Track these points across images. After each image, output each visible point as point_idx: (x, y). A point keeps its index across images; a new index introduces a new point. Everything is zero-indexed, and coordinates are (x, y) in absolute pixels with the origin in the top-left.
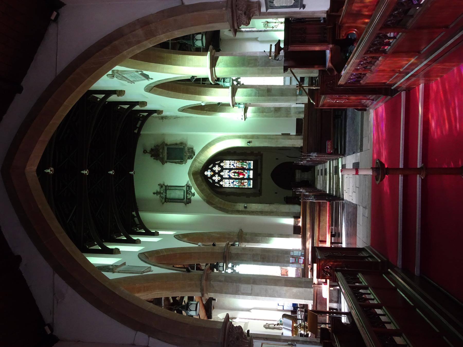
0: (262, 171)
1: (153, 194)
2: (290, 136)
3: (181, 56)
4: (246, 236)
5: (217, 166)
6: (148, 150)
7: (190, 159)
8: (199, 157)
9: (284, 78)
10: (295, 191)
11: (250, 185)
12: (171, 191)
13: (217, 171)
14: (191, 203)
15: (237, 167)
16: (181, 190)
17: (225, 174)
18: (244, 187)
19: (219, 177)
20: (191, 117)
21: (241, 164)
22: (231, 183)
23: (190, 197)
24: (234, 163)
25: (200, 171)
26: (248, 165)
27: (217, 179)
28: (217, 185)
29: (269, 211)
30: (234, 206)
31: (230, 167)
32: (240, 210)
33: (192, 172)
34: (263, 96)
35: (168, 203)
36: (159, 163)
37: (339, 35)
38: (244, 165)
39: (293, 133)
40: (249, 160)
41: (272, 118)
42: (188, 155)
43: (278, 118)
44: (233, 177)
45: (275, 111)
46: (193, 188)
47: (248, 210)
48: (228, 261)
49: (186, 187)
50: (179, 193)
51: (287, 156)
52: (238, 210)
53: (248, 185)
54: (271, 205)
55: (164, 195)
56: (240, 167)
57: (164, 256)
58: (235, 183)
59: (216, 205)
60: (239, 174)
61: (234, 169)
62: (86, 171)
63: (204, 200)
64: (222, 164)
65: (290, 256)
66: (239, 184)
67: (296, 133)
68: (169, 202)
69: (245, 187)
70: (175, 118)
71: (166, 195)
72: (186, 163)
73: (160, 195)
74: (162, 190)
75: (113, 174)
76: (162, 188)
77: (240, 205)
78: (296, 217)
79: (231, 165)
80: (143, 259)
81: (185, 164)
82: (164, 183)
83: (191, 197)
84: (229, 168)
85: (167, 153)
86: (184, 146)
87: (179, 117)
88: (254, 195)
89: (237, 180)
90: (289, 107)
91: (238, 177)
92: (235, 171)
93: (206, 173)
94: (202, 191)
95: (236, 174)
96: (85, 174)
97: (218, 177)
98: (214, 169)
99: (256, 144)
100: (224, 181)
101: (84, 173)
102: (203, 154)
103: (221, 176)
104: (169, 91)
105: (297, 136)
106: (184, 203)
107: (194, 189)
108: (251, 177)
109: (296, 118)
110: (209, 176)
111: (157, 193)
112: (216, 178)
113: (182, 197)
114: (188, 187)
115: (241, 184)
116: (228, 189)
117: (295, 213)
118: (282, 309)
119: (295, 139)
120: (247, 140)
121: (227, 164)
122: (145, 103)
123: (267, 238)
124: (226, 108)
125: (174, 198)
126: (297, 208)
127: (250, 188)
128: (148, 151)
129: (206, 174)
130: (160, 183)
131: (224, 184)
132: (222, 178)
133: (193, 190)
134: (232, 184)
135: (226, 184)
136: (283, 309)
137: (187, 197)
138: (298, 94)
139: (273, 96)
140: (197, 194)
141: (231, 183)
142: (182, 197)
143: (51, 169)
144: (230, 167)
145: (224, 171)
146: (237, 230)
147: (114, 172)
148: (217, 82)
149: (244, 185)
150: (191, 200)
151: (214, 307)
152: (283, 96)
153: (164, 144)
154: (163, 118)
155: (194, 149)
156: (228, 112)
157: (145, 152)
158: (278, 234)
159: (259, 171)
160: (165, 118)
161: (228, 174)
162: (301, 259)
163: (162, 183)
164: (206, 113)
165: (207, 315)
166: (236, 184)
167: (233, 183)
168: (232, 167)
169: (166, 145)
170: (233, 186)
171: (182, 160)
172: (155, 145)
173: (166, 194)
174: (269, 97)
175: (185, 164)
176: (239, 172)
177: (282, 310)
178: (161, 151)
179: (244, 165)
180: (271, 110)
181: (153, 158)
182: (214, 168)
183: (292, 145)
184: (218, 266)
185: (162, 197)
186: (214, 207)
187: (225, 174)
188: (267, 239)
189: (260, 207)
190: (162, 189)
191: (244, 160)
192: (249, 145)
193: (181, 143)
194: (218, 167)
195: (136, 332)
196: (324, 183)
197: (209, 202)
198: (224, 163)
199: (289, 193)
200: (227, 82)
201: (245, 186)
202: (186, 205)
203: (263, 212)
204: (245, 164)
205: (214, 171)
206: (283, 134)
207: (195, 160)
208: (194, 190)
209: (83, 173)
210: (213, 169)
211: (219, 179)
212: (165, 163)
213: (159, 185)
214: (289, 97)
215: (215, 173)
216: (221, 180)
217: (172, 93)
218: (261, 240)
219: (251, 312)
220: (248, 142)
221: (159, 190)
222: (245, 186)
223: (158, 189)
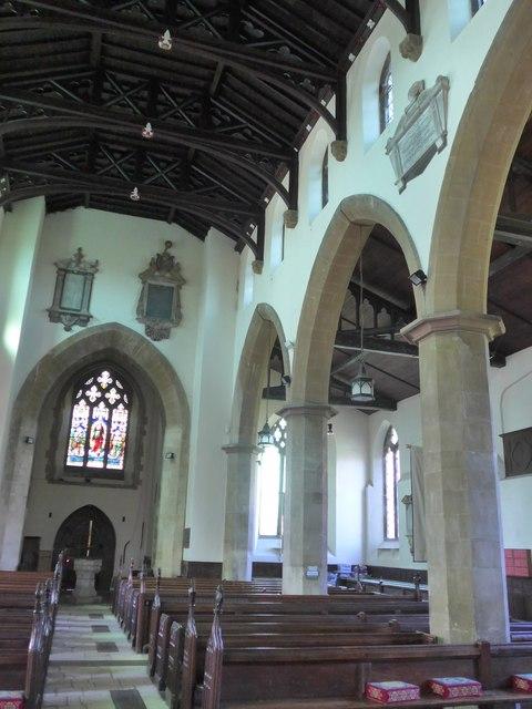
0: (96, 485)
5: (118, 397)
6: (172, 251)
11: (74, 460)
13: (107, 395)
17: (101, 412)
44: (93, 427)
47: (20, 444)
53: (74, 458)
58: (80, 429)
61: (109, 431)
64: (121, 406)
88: (51, 469)
91: (92, 436)
93: (106, 374)
95: (98, 433)
98: (113, 391)
103: (96, 404)
108: (90, 464)
110: (100, 380)
111: (80, 255)
112: (93, 394)
113: (65, 305)
116: (69, 413)
127: (66, 461)
132: (92, 405)
133: (77, 329)
135: (80, 412)
142: (65, 305)
153: (182, 282)
157: (169, 244)
161: (100, 418)
166: (77, 433)
168: (114, 426)
169: (180, 287)
170: (73, 425)
178: (168, 275)
183: (161, 553)
185: (69, 263)
191: (126, 450)
193: (180, 317)
197: (49, 361)
199: (47, 545)
204: (118, 453)
205: (107, 390)
217: (326, 270)
223: (89, 257)
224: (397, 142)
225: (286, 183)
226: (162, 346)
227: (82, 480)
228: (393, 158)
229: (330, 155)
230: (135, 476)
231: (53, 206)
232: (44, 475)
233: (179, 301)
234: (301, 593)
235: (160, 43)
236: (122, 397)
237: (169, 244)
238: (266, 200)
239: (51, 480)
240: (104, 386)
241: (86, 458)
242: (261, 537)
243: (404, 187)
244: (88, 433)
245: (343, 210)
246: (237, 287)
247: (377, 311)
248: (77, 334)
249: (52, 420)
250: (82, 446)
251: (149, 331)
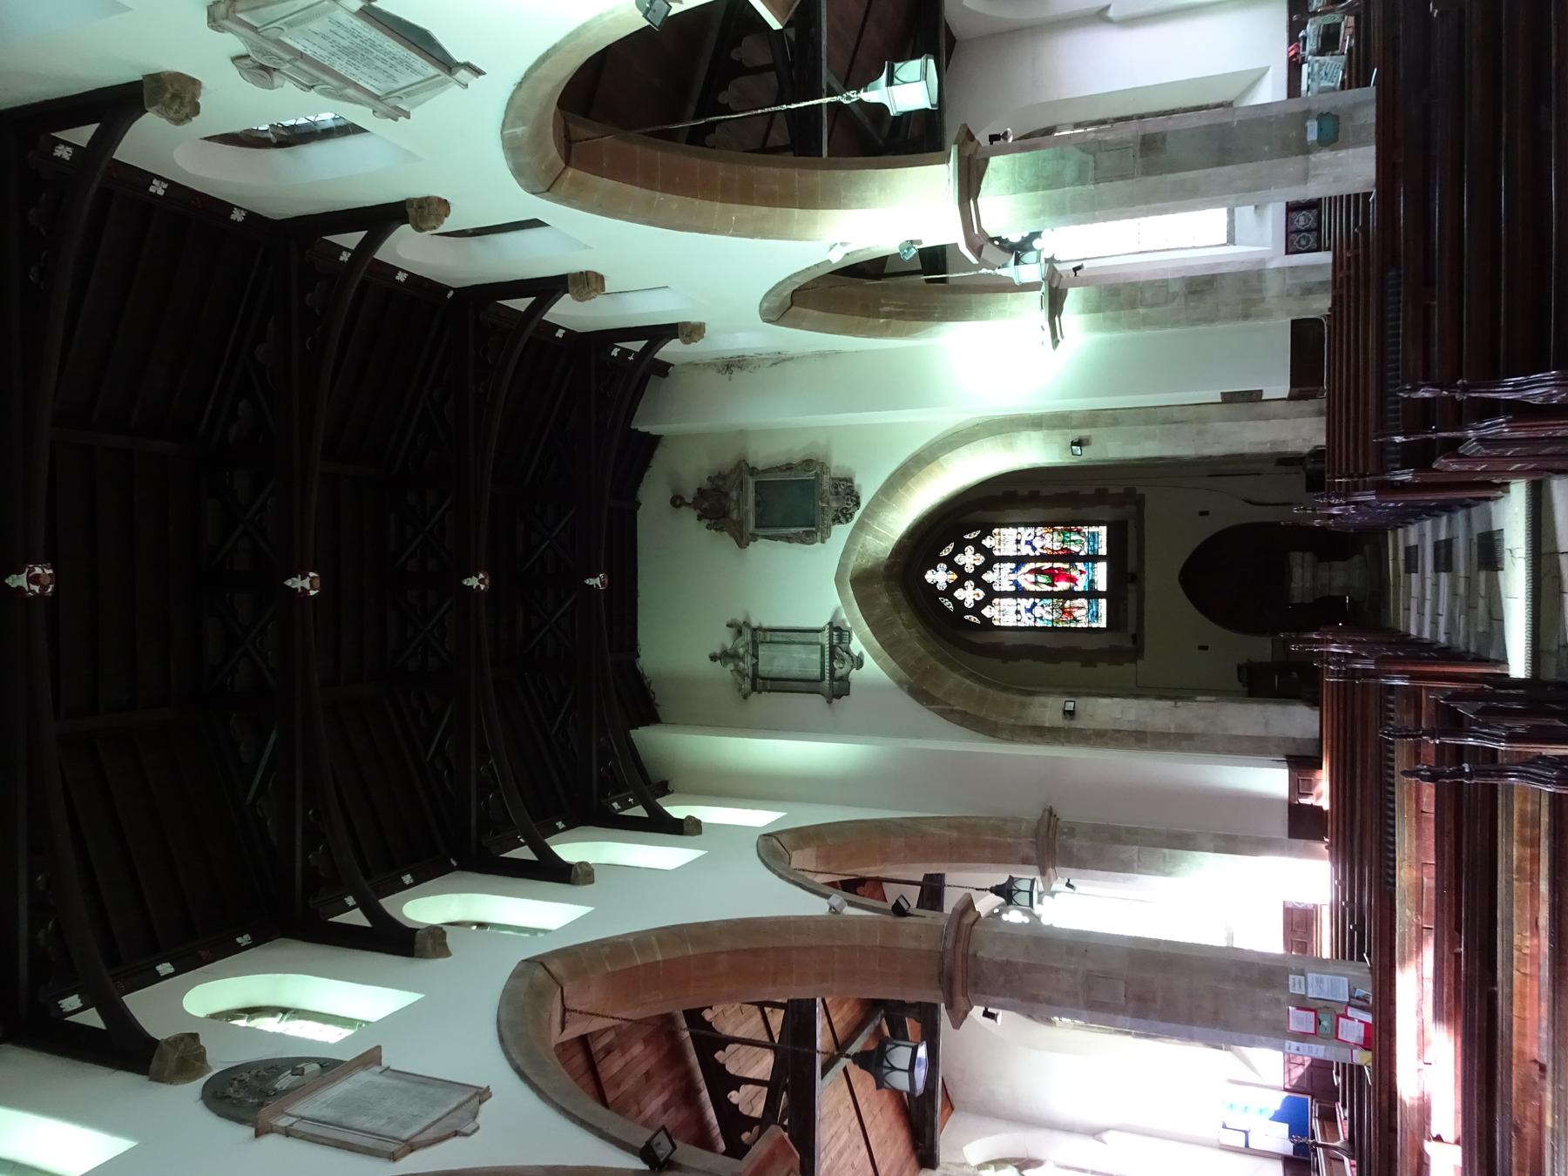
1: (709, 659)
2: (1259, 403)
3: (842, 174)
4: (1070, 841)
5: (970, 549)
6: (690, 493)
7: (840, 522)
8: (875, 512)
9: (1231, 213)
10: (1284, 641)
11: (1096, 616)
12: (774, 647)
14: (848, 694)
15: (1045, 552)
16: (811, 643)
17: (1001, 577)
18: (1073, 625)
19: (979, 591)
20: (837, 353)
21: (1061, 538)
22: (1023, 611)
23: (843, 671)
24: (1035, 536)
25: (882, 569)
26: (1086, 544)
27: (973, 597)
28: (973, 619)
29: (1173, 731)
30: (1023, 706)
31: (1018, 550)
32: (1047, 725)
33: (849, 574)
34: (1122, 177)
35: (763, 693)
36: (726, 541)
37: (1332, 341)
38: (1070, 541)
39: (1277, 386)
40: (1090, 525)
41: (1176, 330)
42: (834, 505)
43: (1203, 328)
44: (1032, 588)
45: (1190, 293)
46: (854, 636)
47: (1077, 724)
48: (965, 995)
49: (827, 631)
50: (804, 656)
51: (1248, 502)
52: (1039, 724)
53: (1091, 616)
54: (1179, 704)
55: (746, 665)
56: (1055, 548)
57: (651, 967)
58: (1038, 611)
59: (950, 705)
60: (1054, 576)
62: (303, 579)
63: (900, 683)
64: (987, 542)
65: (1283, 998)
66: (1055, 615)
67: (1292, 385)
68: (769, 691)
69: (1079, 625)
70: (775, 364)
71: (755, 666)
72: (828, 540)
73: (736, 666)
74: (742, 646)
75: (482, 587)
76: (741, 638)
77: (1044, 706)
78: (1301, 764)
79: (1023, 542)
80: (762, 855)
81: (823, 542)
82: (748, 617)
83: (848, 673)
84: (1015, 554)
85: (757, 504)
86: (819, 472)
87: (791, 359)
88: (1115, 655)
89: (1047, 598)
90: (1257, 268)
91: (1049, 589)
92: (1039, 565)
93: (930, 576)
94: (890, 644)
95: (1041, 579)
96: (300, 590)
97: (974, 589)
98: (959, 559)
99: (1111, 448)
100: (999, 605)
101: (296, 589)
102: (889, 500)
103: (987, 587)
104: (655, 190)
105: (1292, 402)
106: (823, 695)
107: (861, 638)
108: (1102, 586)
109: (1289, 321)
110: (942, 586)
111: (724, 656)
112: (969, 594)
113: (816, 673)
114: (838, 631)
115: (1064, 613)
117: (1294, 739)
118: (1243, 1145)
119: (1285, 418)
120: (1067, 434)
121: (1006, 540)
122: (593, 279)
123: (1166, 851)
124: (970, 303)
125: (784, 676)
126: (1301, 721)
128: (689, 500)
129: (929, 581)
130: (735, 619)
131: (997, 617)
132: (991, 594)
133: (856, 646)
134: (1029, 615)
135: (1005, 614)
136: (1247, 1145)
137: (832, 670)
138: (1315, 138)
139: (1172, 171)
140: (873, 662)
141: (1023, 611)
142: (816, 673)
143: (32, 570)
144: (1018, 550)
145: (996, 566)
146: (1031, 812)
147: (487, 581)
148: (858, 92)
149: (1075, 620)
150: (849, 683)
151: (955, 1099)
152: (1224, 164)
153: (743, 468)
154: (733, 365)
155: (857, 481)
156: (979, 318)
157: (677, 501)
158: (1217, 836)
159: (1132, 564)
160: (741, 368)
161: (1013, 577)
162: (1352, 1019)
163: (741, 620)
164: (887, 326)
165: (920, 1151)
166: (1045, 614)
167: (1030, 610)
168: (1026, 550)
169: (753, 471)
170: (1030, 623)
171: (814, 526)
172: (713, 476)
173: (755, 661)
174: (1153, 180)
175: (823, 542)
176: (1052, 568)
177: (1241, 1148)
178: (734, 495)
179: (1070, 541)
180: (1171, 290)
181: (707, 521)
182: (959, 556)
183: (1273, 443)
184: (1014, 888)
186: (942, 713)
187: (1002, 577)
188: (1165, 857)
189: (1131, 715)
190: (741, 641)
191: (1070, 524)
192: (1079, 452)
193: (808, 463)
194: (974, 554)
195: (671, 1157)
196: (1471, 607)
197: (920, 690)
198: (997, 537)
199: (1261, 649)
200: (905, 83)
201: (1078, 621)
202: (829, 702)
203: (1144, 733)
204: (1075, 537)
205: (959, 569)
206: (1229, 398)
207: (861, 527)
208: (860, 644)
209: (294, 587)
210: (956, 559)
211: (978, 595)
212: (751, 543)
213: (729, 625)
214: (1265, 164)
215: (962, 577)
216: (987, 601)
217: (675, 202)
218: (1139, 858)
219: (1104, 1142)
220: (1073, 444)
221: (729, 645)
222: (1078, 621)
223: (726, 639)
224: (377, 98)
225: (521, 304)
228: (413, 99)
229: (442, 229)
230: (1117, 501)
231: (649, 714)
232: (1128, 668)
233: (779, 469)
234: (1371, 151)
235: (312, 593)
236: (969, 542)
237: (677, 501)
238: (560, 334)
239: (1136, 651)
241: (1091, 594)
242: (1231, 240)
243: (468, 66)
245: (548, 187)
246: (732, 365)
247: (739, 69)
248: (865, 643)
249: (1027, 664)
250: (1068, 604)
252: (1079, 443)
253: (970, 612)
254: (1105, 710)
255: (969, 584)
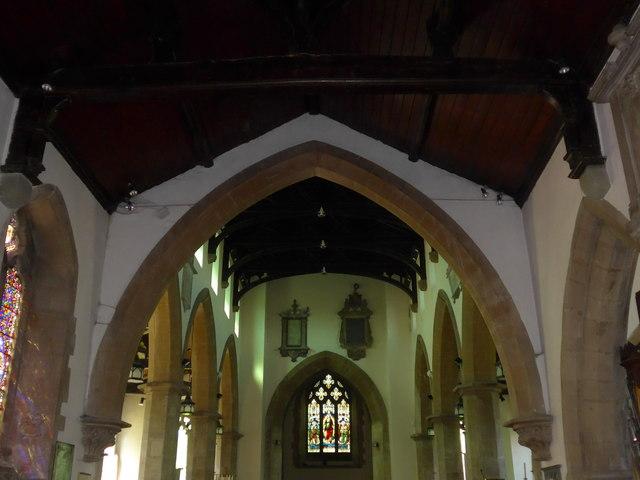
5: (340, 394)
6: (359, 291)
11: (312, 448)
17: (328, 408)
36: (340, 306)
58: (314, 423)
60: (329, 430)
64: (343, 402)
93: (329, 377)
103: (324, 402)
108: (325, 450)
110: (325, 382)
111: (295, 306)
112: (321, 394)
113: (290, 343)
114: (305, 352)
132: (321, 403)
133: (300, 359)
135: (313, 410)
142: (290, 343)
153: (370, 313)
157: (356, 286)
166: (313, 426)
168: (340, 418)
169: (368, 318)
193: (371, 339)
205: (332, 389)
215: (329, 391)
216: (318, 401)
223: (302, 306)
226: (361, 364)
227: (320, 463)
240: (329, 387)
244: (321, 425)
251: (350, 354)
252: (378, 445)
253: (314, 393)
254: (278, 456)
255: (326, 394)
